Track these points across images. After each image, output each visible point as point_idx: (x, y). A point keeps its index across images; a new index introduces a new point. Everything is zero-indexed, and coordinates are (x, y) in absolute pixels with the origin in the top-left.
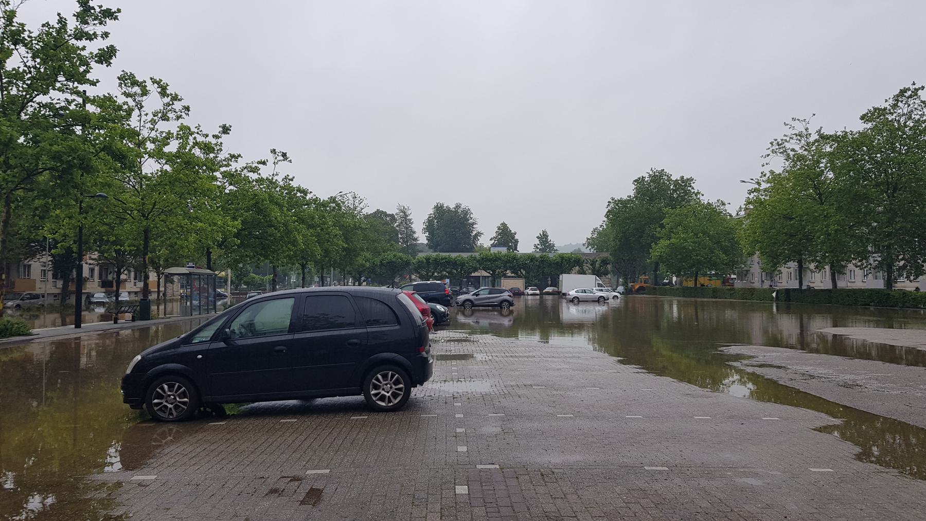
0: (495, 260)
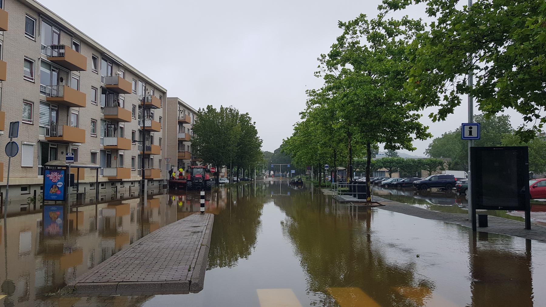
0: (392, 162)
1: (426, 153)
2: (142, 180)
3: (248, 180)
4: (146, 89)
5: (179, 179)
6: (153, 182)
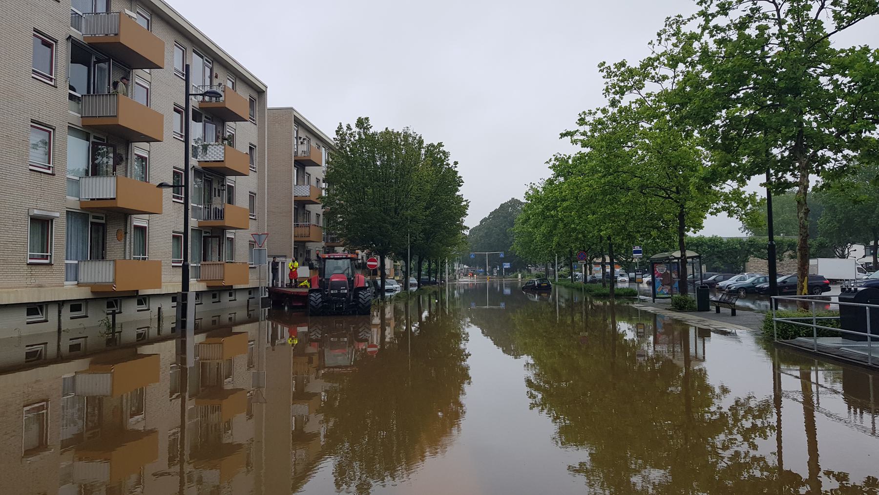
0: (701, 245)
1: (743, 230)
3: (435, 283)
4: (214, 75)
6: (233, 295)
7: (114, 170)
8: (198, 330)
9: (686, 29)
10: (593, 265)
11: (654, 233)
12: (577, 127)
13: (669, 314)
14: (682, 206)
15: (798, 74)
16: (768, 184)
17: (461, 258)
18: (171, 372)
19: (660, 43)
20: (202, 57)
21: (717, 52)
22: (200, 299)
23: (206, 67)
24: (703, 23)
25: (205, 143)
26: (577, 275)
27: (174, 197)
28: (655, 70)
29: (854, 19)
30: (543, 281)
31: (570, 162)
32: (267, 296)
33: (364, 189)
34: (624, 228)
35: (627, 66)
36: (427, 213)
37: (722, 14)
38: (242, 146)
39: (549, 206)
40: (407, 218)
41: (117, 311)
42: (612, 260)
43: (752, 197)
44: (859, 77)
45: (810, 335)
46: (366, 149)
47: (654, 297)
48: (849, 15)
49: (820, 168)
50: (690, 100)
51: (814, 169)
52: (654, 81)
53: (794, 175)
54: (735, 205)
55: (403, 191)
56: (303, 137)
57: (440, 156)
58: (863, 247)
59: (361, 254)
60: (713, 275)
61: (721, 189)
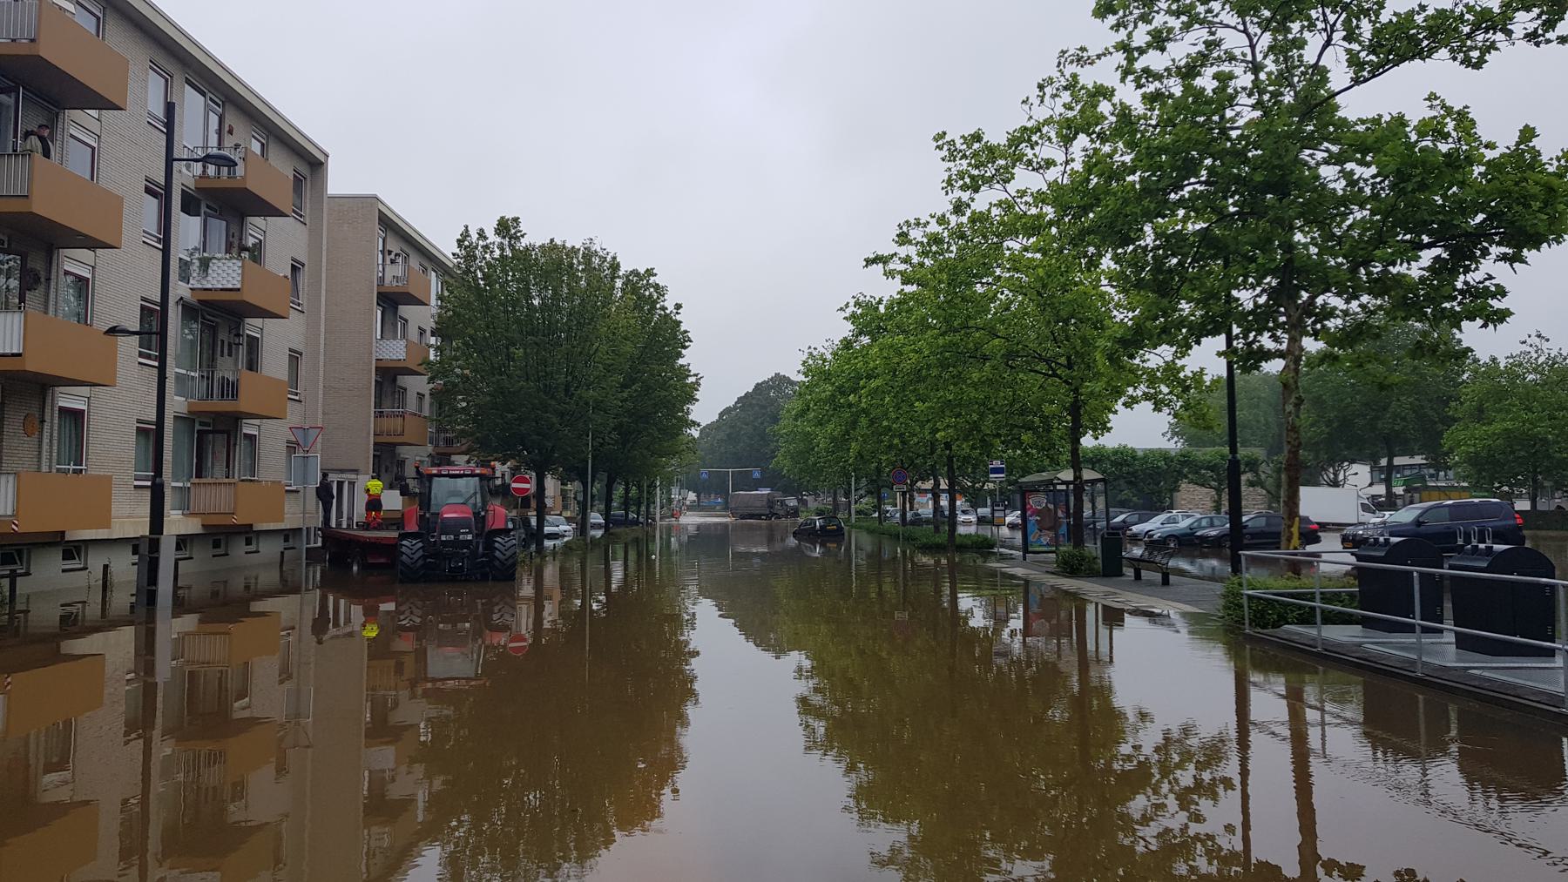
0: (1099, 461)
1: (1169, 435)
2: (151, 540)
3: (636, 522)
4: (227, 129)
5: (365, 526)
6: (254, 542)
7: (22, 299)
8: (180, 606)
9: (1089, 77)
10: (915, 493)
11: (1026, 437)
12: (894, 248)
13: (1052, 581)
14: (1076, 391)
15: (1285, 160)
16: (1230, 351)
17: (683, 478)
18: (127, 688)
19: (1042, 101)
20: (203, 94)
21: (1145, 117)
22: (25, 564)
23: (211, 113)
24: (1124, 63)
25: (205, 255)
26: (888, 511)
27: (141, 355)
28: (1033, 149)
29: (1383, 66)
30: (830, 521)
31: (882, 309)
32: (319, 544)
33: (508, 349)
34: (975, 426)
35: (985, 140)
36: (625, 395)
37: (1156, 48)
38: (277, 262)
39: (843, 387)
40: (587, 404)
41: (18, 571)
42: (951, 485)
43: (1198, 376)
44: (1392, 167)
45: (1307, 618)
46: (514, 275)
47: (1026, 550)
48: (1372, 57)
49: (1319, 326)
50: (1098, 200)
51: (1309, 328)
52: (1030, 168)
53: (1275, 338)
54: (1165, 390)
55: (581, 353)
56: (396, 250)
57: (651, 294)
58: (1368, 468)
59: (501, 469)
60: (1122, 513)
61: (1143, 361)
